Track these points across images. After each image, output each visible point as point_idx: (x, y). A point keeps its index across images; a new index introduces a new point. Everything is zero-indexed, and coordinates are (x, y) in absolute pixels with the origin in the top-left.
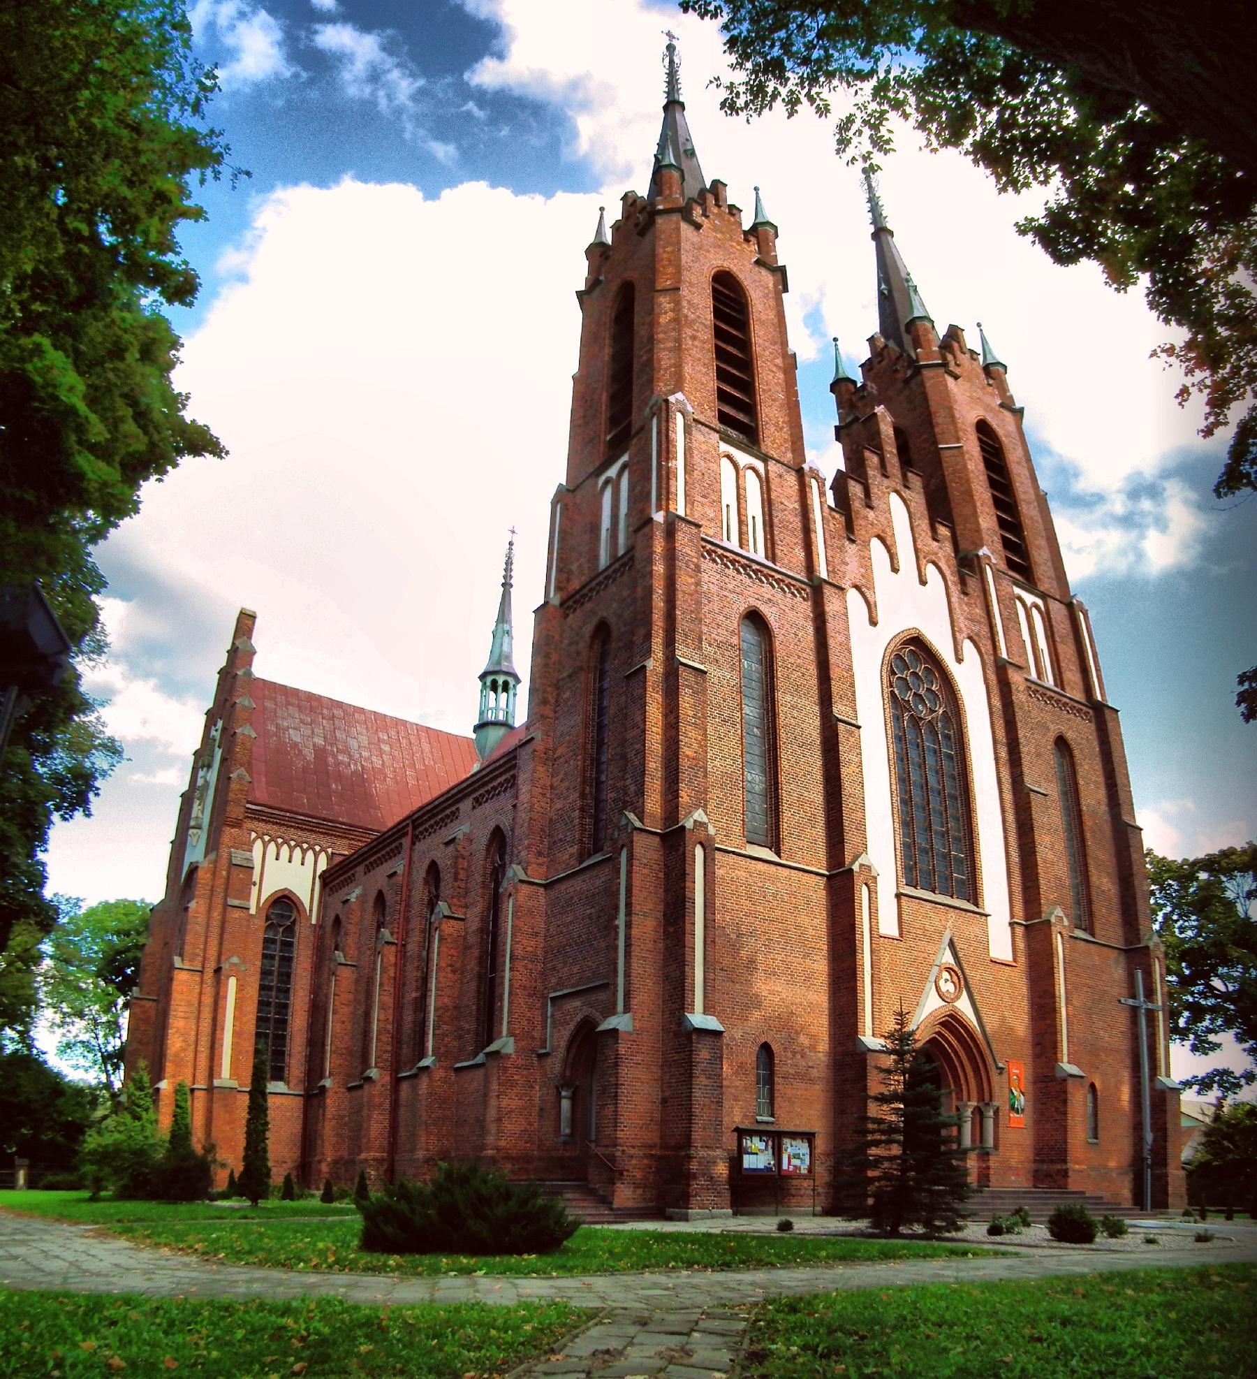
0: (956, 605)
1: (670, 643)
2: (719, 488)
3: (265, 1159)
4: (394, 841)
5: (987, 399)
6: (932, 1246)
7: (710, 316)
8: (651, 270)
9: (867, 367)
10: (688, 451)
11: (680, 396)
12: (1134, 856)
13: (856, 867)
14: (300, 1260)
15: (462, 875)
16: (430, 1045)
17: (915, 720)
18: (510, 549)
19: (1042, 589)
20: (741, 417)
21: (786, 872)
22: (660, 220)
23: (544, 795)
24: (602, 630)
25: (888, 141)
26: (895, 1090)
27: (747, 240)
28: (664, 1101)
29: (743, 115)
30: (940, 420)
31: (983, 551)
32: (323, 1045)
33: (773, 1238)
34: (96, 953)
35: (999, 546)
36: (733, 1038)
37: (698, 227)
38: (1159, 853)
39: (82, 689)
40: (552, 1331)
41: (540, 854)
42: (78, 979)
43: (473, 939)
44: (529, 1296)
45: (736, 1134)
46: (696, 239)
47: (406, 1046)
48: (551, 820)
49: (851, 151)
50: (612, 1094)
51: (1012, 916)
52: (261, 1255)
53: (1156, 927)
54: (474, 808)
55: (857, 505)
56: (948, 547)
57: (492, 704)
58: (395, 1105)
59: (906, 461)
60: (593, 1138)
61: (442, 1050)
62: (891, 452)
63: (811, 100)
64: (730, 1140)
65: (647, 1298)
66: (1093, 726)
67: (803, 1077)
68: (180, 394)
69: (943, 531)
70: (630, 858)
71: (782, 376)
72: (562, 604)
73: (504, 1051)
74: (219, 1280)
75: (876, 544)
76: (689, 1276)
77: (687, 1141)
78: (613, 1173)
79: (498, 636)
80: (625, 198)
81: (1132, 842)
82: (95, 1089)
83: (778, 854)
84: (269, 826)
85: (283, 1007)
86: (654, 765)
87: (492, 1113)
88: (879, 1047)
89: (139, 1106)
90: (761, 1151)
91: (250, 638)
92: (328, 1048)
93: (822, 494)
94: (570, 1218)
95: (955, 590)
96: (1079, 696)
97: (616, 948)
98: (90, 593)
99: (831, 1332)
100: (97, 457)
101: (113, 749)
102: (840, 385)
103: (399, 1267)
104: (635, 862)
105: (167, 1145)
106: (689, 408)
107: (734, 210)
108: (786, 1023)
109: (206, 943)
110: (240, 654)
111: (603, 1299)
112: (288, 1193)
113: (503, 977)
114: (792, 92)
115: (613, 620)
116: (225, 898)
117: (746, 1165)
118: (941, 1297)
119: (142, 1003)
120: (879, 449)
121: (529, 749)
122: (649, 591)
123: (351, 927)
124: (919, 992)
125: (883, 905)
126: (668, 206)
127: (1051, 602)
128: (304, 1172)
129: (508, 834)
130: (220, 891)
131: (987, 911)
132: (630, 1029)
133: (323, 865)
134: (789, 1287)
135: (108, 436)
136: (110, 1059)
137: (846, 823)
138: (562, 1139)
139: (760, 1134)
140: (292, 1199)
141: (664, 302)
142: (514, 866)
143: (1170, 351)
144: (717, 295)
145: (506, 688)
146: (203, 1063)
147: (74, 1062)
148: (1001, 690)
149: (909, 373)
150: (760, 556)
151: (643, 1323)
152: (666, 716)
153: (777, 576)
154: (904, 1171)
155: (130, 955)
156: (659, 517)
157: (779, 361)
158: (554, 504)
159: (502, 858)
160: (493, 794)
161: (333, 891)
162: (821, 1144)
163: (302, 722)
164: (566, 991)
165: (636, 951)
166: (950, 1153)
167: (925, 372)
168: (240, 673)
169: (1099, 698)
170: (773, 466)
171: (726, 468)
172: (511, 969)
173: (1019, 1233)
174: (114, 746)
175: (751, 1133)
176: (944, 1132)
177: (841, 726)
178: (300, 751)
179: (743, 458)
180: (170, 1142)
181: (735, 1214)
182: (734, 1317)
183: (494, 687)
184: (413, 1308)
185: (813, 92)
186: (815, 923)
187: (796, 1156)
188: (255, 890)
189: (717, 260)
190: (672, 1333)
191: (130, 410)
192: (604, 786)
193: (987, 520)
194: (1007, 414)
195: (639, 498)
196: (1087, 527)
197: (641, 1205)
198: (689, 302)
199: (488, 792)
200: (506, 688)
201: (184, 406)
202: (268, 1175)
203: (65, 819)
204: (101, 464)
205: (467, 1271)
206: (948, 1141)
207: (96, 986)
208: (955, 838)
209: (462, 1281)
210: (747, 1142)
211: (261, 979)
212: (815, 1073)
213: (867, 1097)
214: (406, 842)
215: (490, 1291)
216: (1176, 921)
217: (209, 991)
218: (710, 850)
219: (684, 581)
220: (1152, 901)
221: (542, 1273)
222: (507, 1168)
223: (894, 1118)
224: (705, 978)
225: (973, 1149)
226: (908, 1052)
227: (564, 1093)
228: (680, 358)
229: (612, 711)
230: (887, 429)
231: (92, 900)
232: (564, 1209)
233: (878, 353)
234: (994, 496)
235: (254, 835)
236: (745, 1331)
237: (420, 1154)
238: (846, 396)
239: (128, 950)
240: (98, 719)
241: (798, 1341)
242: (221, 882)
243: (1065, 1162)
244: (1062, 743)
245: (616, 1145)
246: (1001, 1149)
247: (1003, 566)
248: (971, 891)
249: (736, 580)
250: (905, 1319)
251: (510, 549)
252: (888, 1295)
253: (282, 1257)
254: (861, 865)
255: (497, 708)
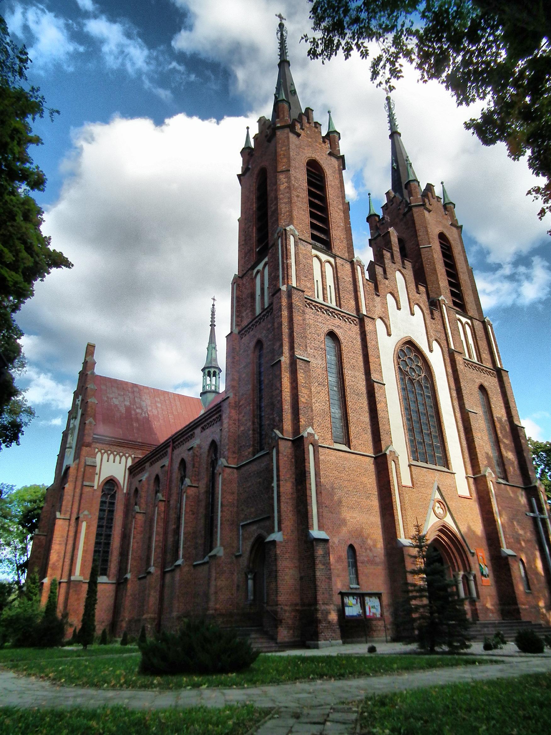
0: (428, 325)
1: (292, 348)
2: (314, 273)
3: (93, 620)
4: (164, 450)
6: (455, 659)
7: (305, 185)
8: (275, 160)
9: (385, 208)
10: (296, 255)
11: (292, 227)
12: (523, 441)
13: (388, 452)
14: (105, 682)
15: (197, 465)
16: (181, 553)
18: (213, 308)
19: (470, 315)
20: (322, 236)
22: (278, 133)
23: (235, 424)
24: (259, 344)
25: (400, 71)
26: (420, 568)
27: (324, 142)
28: (301, 578)
29: (320, 58)
30: (421, 234)
31: (442, 298)
32: (128, 555)
33: (367, 658)
34: (19, 512)
35: (449, 295)
36: (334, 543)
37: (298, 135)
38: (535, 439)
39: (15, 385)
40: (244, 725)
41: (234, 452)
42: (9, 526)
43: (202, 497)
44: (231, 701)
45: (340, 596)
46: (297, 143)
47: (170, 552)
48: (239, 436)
49: (379, 79)
50: (274, 575)
51: (467, 473)
52: (85, 680)
53: (538, 476)
54: (202, 432)
55: (380, 277)
56: (424, 296)
57: (208, 382)
58: (163, 586)
59: (404, 255)
60: (265, 601)
61: (187, 556)
63: (358, 47)
64: (337, 599)
65: (298, 700)
66: (496, 380)
67: (372, 562)
68: (46, 237)
69: (422, 289)
70: (278, 453)
71: (342, 214)
72: (239, 333)
73: (218, 555)
74: (59, 697)
75: (389, 297)
76: (321, 684)
77: (315, 602)
78: (277, 621)
79: (210, 349)
80: (259, 121)
81: (521, 434)
82: (11, 584)
83: (350, 448)
84: (104, 446)
85: (109, 536)
86: (287, 407)
87: (212, 590)
88: (408, 544)
89: (32, 593)
90: (354, 605)
91: (93, 356)
92: (130, 557)
93: (363, 273)
94: (254, 650)
95: (428, 317)
96: (489, 365)
97: (273, 498)
98: (16, 339)
99: (407, 718)
100: (10, 270)
101: (30, 412)
102: (371, 218)
103: (159, 684)
104: (280, 455)
105: (43, 614)
106: (297, 233)
107: (317, 125)
108: (359, 533)
109: (72, 505)
110: (88, 365)
111: (273, 701)
112: (103, 641)
113: (217, 515)
114: (347, 43)
115: (264, 339)
116: (83, 482)
117: (347, 613)
118: (467, 691)
119: (40, 537)
120: (390, 250)
121: (227, 402)
122: (281, 324)
123: (143, 494)
124: (426, 513)
125: (402, 471)
126: (283, 124)
127: (474, 321)
128: (113, 626)
129: (218, 443)
130: (80, 478)
131: (454, 471)
132: (282, 540)
133: (130, 463)
134: (379, 689)
135: (14, 259)
136: (21, 567)
138: (249, 602)
139: (353, 595)
140: (105, 644)
141: (282, 178)
142: (222, 459)
143: (537, 190)
144: (309, 173)
145: (215, 375)
146: (67, 568)
147: (3, 570)
148: (451, 364)
149: (406, 210)
150: (334, 305)
151: (297, 716)
152: (291, 383)
154: (431, 613)
155: (36, 512)
156: (284, 288)
157: (341, 207)
158: (233, 284)
159: (216, 455)
160: (210, 425)
161: (134, 476)
162: (386, 599)
163: (119, 395)
164: (248, 522)
165: (283, 499)
166: (454, 602)
167: (414, 210)
168: (89, 373)
169: (499, 366)
170: (339, 261)
171: (316, 262)
172: (221, 511)
173: (501, 648)
174: (31, 411)
175: (348, 595)
176: (449, 590)
177: (376, 384)
178: (118, 409)
179: (324, 257)
180: (46, 612)
181: (344, 643)
182: (349, 710)
183: (209, 375)
184: (165, 711)
185: (359, 42)
186: (370, 480)
187: (373, 607)
188: (97, 477)
189: (309, 154)
190: (315, 723)
191: (23, 245)
192: (263, 418)
193: (443, 282)
194: (454, 229)
195: (274, 279)
196: (492, 282)
197: (292, 640)
198: (295, 177)
199: (208, 424)
200: (215, 375)
201: (49, 243)
202: (94, 630)
203: (8, 447)
204: (13, 273)
205: (196, 686)
206: (452, 594)
207: (18, 529)
208: (435, 436)
209: (194, 692)
210: (346, 600)
211: (99, 522)
212: (378, 560)
213: (405, 572)
214: (169, 450)
215: (209, 698)
216: (547, 473)
217: (72, 530)
218: (316, 447)
219: (297, 318)
220: (534, 463)
221: (239, 685)
222: (220, 621)
223: (421, 583)
224: (318, 511)
225: (466, 599)
226: (424, 546)
227: (249, 576)
228: (291, 207)
229: (266, 381)
230: (394, 239)
231: (19, 486)
232: (251, 644)
233: (391, 200)
234: (446, 270)
235: (97, 450)
236: (356, 720)
237: (175, 614)
238: (374, 224)
239: (35, 509)
240: (23, 398)
241: (389, 726)
242: (80, 474)
243: (516, 604)
244: (482, 388)
245: (277, 605)
246: (481, 598)
247: (451, 305)
248: (446, 462)
249: (322, 316)
250: (448, 707)
251: (213, 308)
252: (436, 692)
253: (96, 680)
255: (211, 385)
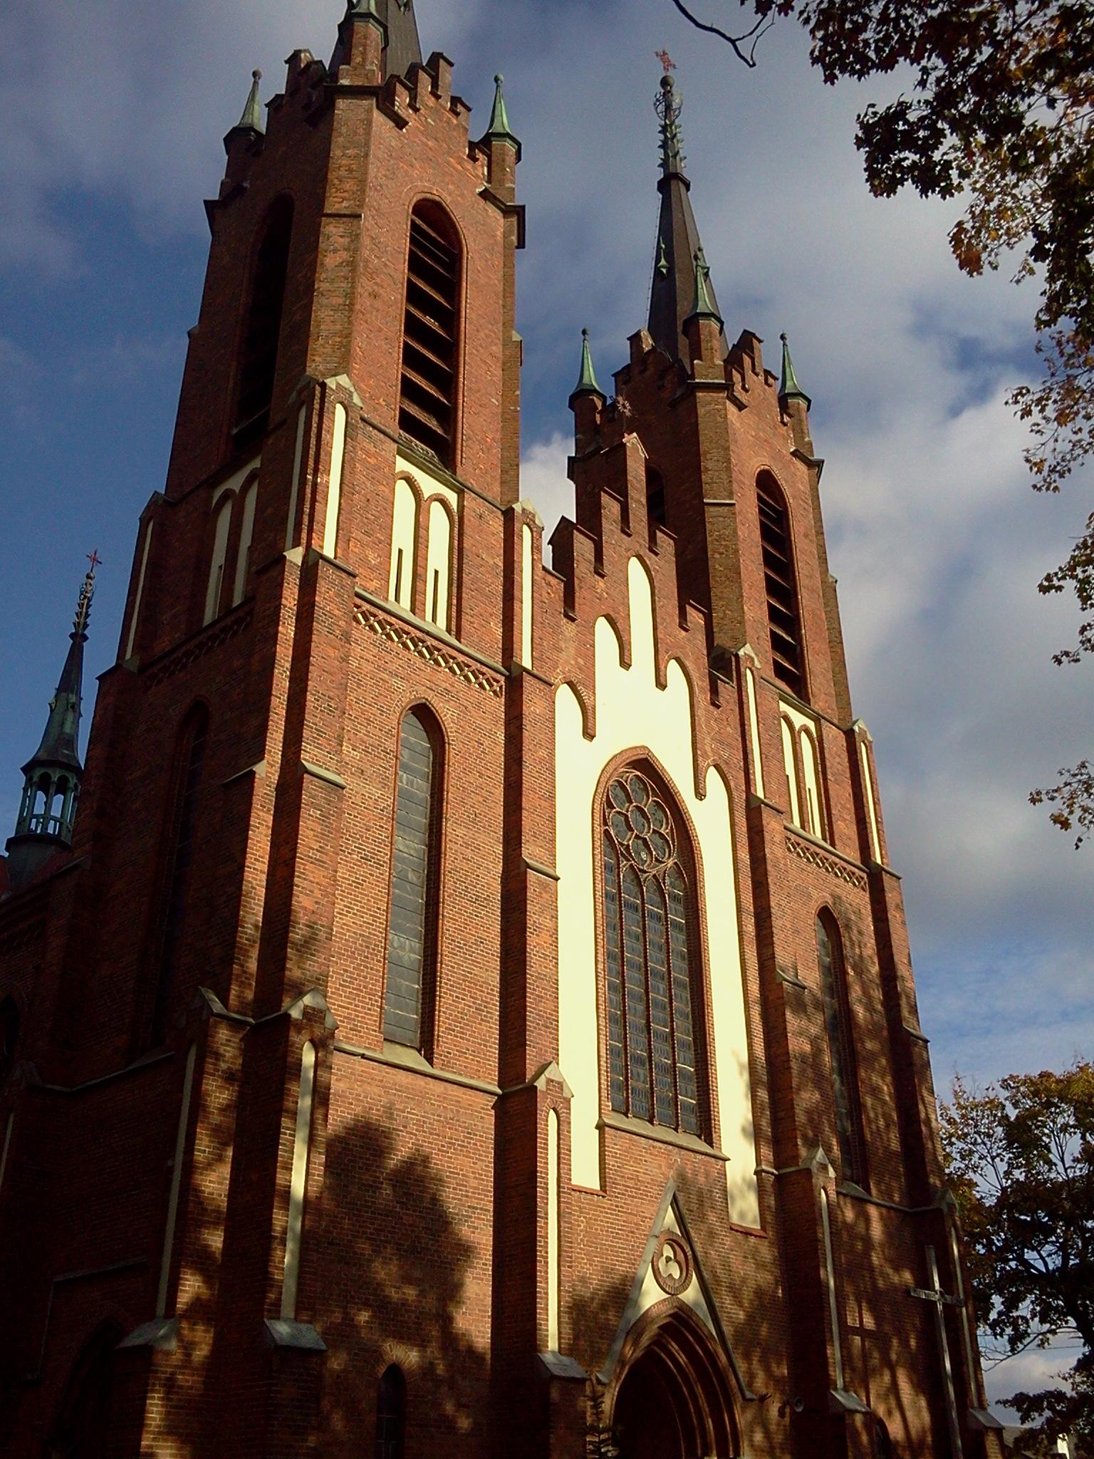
0: (701, 720)
2: (390, 527)
5: (778, 443)
11: (343, 380)
13: (541, 1084)
17: (635, 873)
19: (816, 708)
20: (433, 424)
21: (439, 1087)
30: (710, 465)
37: (400, 123)
51: (758, 1162)
59: (657, 517)
62: (639, 501)
69: (696, 618)
75: (602, 625)
83: (429, 1059)
91: (628, 367)
95: (703, 698)
96: (853, 855)
106: (356, 400)
137: (530, 1016)
141: (333, 232)
153: (461, 658)
157: (497, 349)
158: (144, 522)
169: (879, 861)
177: (532, 875)
179: (430, 486)
193: (756, 607)
219: (322, 651)
228: (350, 323)
234: (767, 577)
244: (826, 917)
247: (770, 673)
248: (706, 1127)
254: (549, 1081)
